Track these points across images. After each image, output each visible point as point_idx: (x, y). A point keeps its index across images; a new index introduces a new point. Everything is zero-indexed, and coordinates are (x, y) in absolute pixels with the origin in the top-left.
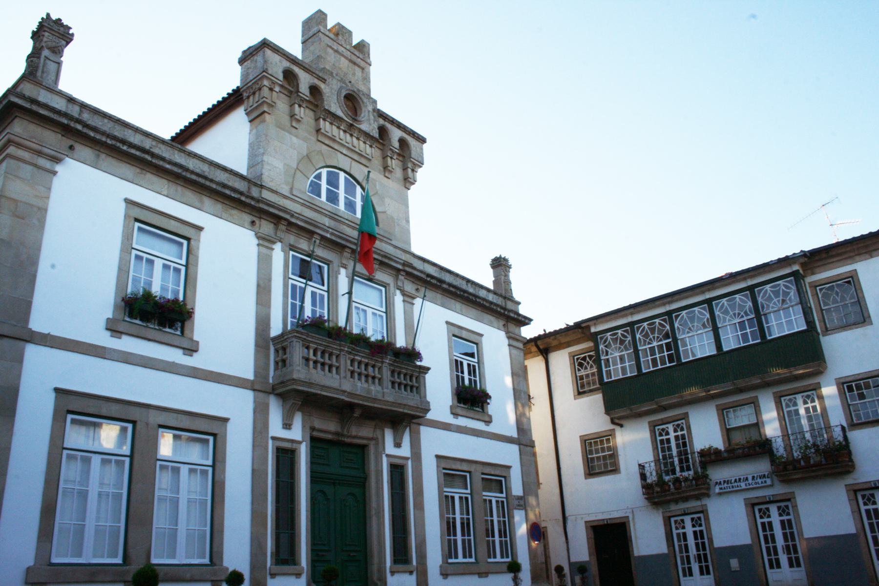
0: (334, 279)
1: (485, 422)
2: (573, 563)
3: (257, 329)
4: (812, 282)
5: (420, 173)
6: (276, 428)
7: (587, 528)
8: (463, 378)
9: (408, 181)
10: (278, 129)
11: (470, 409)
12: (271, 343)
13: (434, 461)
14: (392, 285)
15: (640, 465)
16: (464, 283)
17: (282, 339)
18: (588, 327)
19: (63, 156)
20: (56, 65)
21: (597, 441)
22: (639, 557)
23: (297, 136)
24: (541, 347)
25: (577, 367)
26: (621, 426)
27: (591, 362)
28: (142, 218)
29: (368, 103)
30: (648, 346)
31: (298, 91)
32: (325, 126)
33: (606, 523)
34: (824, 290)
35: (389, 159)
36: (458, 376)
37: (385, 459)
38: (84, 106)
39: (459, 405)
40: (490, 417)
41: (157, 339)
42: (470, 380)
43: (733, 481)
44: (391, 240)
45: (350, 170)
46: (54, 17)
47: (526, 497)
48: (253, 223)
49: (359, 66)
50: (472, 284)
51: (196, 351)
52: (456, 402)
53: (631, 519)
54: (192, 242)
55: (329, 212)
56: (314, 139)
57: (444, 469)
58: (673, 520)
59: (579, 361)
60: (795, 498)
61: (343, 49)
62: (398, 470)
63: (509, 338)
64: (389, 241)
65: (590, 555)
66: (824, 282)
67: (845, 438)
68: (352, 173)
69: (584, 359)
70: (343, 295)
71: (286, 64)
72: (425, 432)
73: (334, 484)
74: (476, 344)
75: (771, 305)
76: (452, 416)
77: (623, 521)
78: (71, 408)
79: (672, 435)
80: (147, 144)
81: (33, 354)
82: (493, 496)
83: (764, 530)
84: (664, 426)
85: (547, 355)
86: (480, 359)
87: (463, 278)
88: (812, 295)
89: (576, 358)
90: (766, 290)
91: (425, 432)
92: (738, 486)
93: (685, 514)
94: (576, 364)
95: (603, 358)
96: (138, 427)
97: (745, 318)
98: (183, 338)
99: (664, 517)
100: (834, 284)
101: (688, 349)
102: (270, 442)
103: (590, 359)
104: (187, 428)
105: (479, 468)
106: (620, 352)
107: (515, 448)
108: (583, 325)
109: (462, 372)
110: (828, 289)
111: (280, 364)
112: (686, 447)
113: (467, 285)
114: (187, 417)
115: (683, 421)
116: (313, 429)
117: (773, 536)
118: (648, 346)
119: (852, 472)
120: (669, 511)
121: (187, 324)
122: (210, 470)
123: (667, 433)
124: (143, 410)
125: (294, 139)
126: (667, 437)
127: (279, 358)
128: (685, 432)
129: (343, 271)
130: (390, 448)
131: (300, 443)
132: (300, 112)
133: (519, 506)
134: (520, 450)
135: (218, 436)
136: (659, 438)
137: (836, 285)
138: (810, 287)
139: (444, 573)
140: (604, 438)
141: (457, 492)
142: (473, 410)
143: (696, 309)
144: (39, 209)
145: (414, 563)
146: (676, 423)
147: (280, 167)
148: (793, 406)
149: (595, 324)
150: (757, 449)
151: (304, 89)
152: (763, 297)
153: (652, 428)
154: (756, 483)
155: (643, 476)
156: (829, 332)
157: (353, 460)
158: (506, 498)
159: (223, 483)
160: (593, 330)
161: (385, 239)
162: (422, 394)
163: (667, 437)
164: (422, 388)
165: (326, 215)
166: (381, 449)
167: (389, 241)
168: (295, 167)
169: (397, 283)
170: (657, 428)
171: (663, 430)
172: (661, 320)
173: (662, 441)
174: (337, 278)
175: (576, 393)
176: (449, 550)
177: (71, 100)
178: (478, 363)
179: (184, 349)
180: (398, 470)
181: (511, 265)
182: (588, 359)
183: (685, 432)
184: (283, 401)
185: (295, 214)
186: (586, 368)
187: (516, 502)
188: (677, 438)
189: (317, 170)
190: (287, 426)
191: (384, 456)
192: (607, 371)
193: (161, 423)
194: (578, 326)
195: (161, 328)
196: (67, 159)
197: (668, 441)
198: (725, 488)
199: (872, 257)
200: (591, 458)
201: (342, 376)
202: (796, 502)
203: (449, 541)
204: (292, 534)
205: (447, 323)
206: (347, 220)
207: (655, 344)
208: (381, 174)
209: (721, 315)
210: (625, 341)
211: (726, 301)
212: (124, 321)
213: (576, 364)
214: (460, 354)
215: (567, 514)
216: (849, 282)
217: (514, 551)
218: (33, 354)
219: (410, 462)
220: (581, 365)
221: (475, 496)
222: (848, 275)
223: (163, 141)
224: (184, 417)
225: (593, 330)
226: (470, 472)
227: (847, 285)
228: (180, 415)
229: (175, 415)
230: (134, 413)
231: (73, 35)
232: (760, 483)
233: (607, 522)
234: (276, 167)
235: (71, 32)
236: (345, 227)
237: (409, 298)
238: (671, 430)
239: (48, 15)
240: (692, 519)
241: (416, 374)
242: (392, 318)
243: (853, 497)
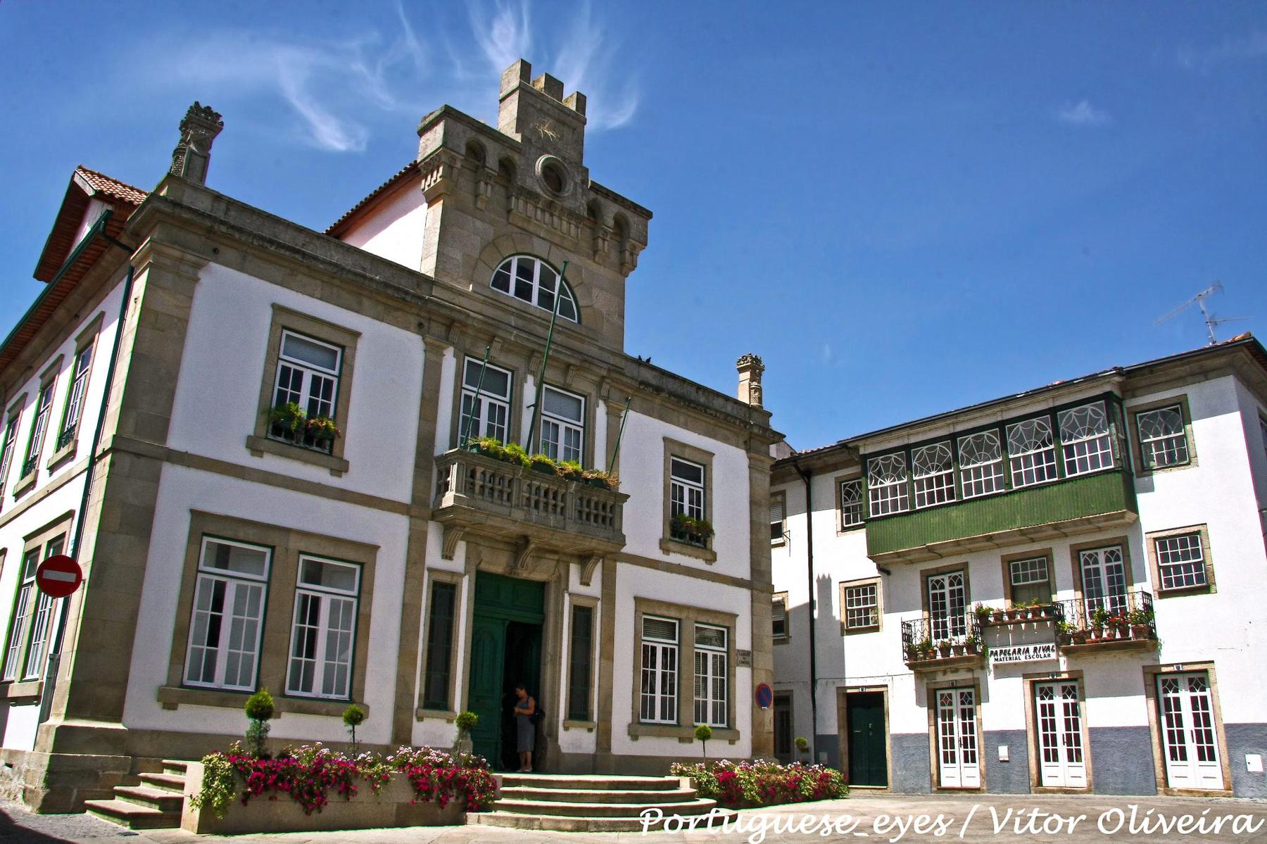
0: (519, 387)
2: (819, 736)
4: (1132, 407)
5: (643, 257)
8: (682, 507)
9: (625, 266)
10: (458, 213)
11: (688, 544)
12: (434, 463)
13: (631, 605)
14: (594, 394)
16: (693, 390)
18: (857, 449)
19: (206, 262)
20: (202, 160)
23: (482, 220)
24: (802, 469)
28: (291, 326)
29: (576, 173)
30: (924, 476)
31: (484, 166)
32: (518, 205)
34: (1144, 419)
35: (600, 241)
36: (674, 505)
37: (567, 597)
38: (231, 203)
39: (672, 538)
40: (714, 555)
42: (691, 509)
43: (1011, 652)
44: (597, 341)
46: (203, 105)
47: (755, 652)
48: (420, 325)
49: (569, 126)
50: (704, 391)
52: (668, 536)
54: (347, 350)
55: (516, 309)
56: (503, 221)
58: (939, 693)
60: (1082, 678)
61: (548, 106)
62: (582, 617)
64: (595, 343)
65: (839, 728)
66: (1146, 408)
67: (1149, 608)
68: (551, 260)
71: (471, 134)
72: (622, 569)
75: (1075, 434)
78: (206, 531)
79: (947, 590)
80: (301, 239)
81: (172, 474)
82: (711, 651)
83: (1044, 714)
84: (939, 578)
85: (809, 479)
86: (707, 483)
87: (692, 384)
88: (1130, 425)
90: (1071, 416)
91: (622, 569)
92: (1016, 659)
93: (956, 688)
95: (871, 487)
96: (277, 553)
97: (1042, 449)
98: (330, 458)
99: (928, 689)
100: (1158, 411)
101: (1074, 460)
102: (426, 573)
105: (692, 615)
106: (1037, 449)
107: (745, 594)
108: (850, 445)
109: (682, 499)
110: (1149, 417)
112: (933, 604)
113: (697, 392)
115: (962, 573)
117: (1053, 722)
118: (924, 476)
119: (1149, 651)
120: (935, 683)
121: (337, 443)
122: (355, 601)
123: (942, 587)
125: (479, 224)
126: (942, 591)
127: (442, 481)
128: (962, 586)
129: (530, 379)
130: (574, 584)
131: (461, 576)
132: (486, 190)
134: (752, 596)
136: (931, 592)
137: (1161, 412)
138: (1128, 413)
141: (660, 644)
142: (691, 545)
143: (985, 433)
144: (180, 319)
145: (595, 719)
146: (954, 574)
147: (458, 258)
148: (1093, 563)
150: (1043, 614)
151: (492, 162)
152: (1065, 424)
153: (924, 579)
154: (1037, 656)
155: (907, 638)
156: (1145, 473)
158: (728, 652)
159: (368, 617)
162: (617, 527)
163: (942, 591)
164: (617, 520)
165: (512, 314)
166: (563, 586)
167: (595, 343)
168: (476, 256)
170: (930, 579)
171: (937, 582)
172: (991, 433)
173: (935, 596)
174: (522, 387)
175: (840, 529)
176: (645, 708)
177: (218, 197)
178: (704, 488)
180: (582, 617)
183: (962, 586)
185: (472, 314)
186: (854, 498)
187: (741, 658)
188: (952, 593)
189: (505, 259)
190: (448, 555)
193: (303, 549)
194: (843, 446)
195: (307, 446)
196: (212, 264)
197: (943, 595)
198: (1001, 660)
199: (1207, 379)
201: (513, 503)
202: (1083, 683)
203: (644, 698)
205: (665, 439)
206: (539, 318)
207: (933, 474)
208: (589, 259)
209: (1014, 443)
210: (1099, 420)
211: (1022, 425)
212: (267, 438)
215: (817, 677)
216: (1176, 410)
217: (732, 716)
218: (172, 474)
219: (599, 603)
220: (848, 494)
221: (684, 649)
222: (1176, 401)
223: (318, 236)
225: (862, 451)
226: (680, 620)
227: (1173, 413)
230: (274, 539)
231: (222, 124)
232: (1042, 656)
234: (452, 258)
235: (221, 120)
236: (537, 327)
238: (946, 583)
239: (197, 103)
240: (962, 694)
241: (610, 503)
242: (591, 433)
243: (1150, 681)
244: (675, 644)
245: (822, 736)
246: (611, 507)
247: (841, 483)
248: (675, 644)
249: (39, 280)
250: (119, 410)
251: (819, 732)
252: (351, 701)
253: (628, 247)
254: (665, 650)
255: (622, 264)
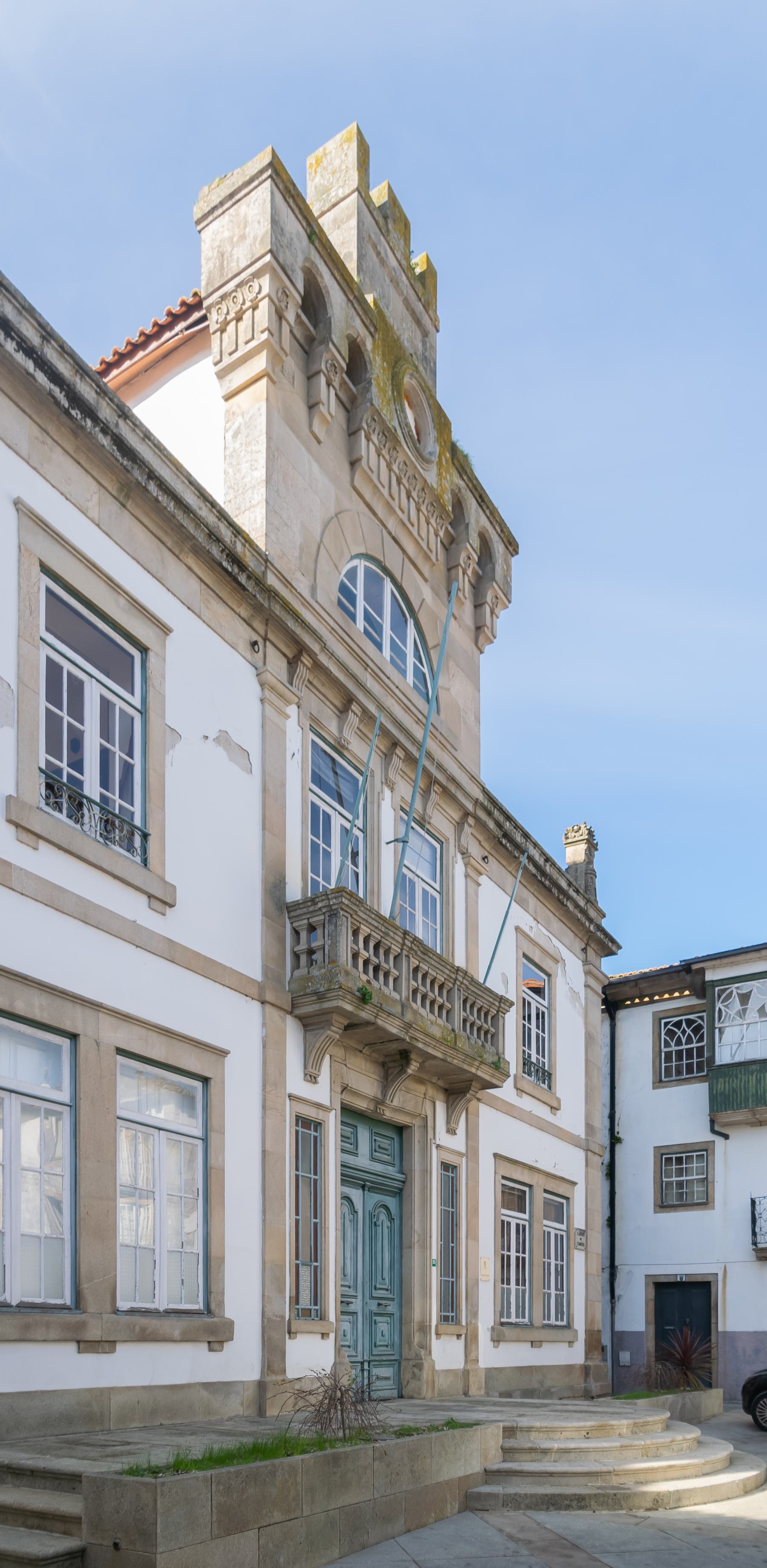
1: (552, 1108)
3: (265, 881)
6: (295, 1083)
7: (647, 1285)
15: (752, 1199)
17: (311, 909)
18: (702, 971)
21: (672, 1158)
22: (725, 1333)
25: (663, 1036)
26: (726, 1137)
27: (689, 1031)
33: (679, 1280)
40: (558, 1100)
41: (105, 866)
45: (91, 794)
51: (171, 906)
53: (720, 1278)
57: (504, 1178)
59: (669, 1027)
63: (587, 973)
69: (678, 1025)
70: (388, 843)
73: (363, 1187)
74: (549, 975)
76: (515, 1090)
77: (709, 1279)
89: (663, 1021)
91: (485, 1113)
94: (663, 1033)
103: (689, 1026)
104: (162, 1060)
108: (695, 967)
111: (303, 959)
114: (164, 1038)
116: (345, 1089)
124: (89, 1013)
133: (580, 1244)
135: (212, 1083)
139: (495, 1339)
140: (695, 1154)
149: (714, 968)
157: (386, 1150)
160: (710, 976)
161: (448, 746)
169: (459, 840)
176: (503, 1309)
179: (150, 896)
181: (597, 844)
182: (684, 1025)
184: (305, 1031)
191: (434, 1147)
192: (666, 1053)
194: (687, 967)
200: (667, 1183)
204: (316, 1268)
213: (663, 1033)
214: (529, 988)
220: (671, 1034)
221: (536, 1226)
224: (153, 1036)
228: (151, 1033)
229: (143, 1032)
233: (681, 1278)
237: (472, 877)
244: (525, 1220)
245: (623, 1332)
246: (493, 1018)
247: (660, 1019)
248: (525, 1220)
249: (436, 273)
250: (343, 612)
251: (618, 1328)
252: (208, 1311)
253: (489, 598)
254: (518, 1225)
255: (478, 628)
